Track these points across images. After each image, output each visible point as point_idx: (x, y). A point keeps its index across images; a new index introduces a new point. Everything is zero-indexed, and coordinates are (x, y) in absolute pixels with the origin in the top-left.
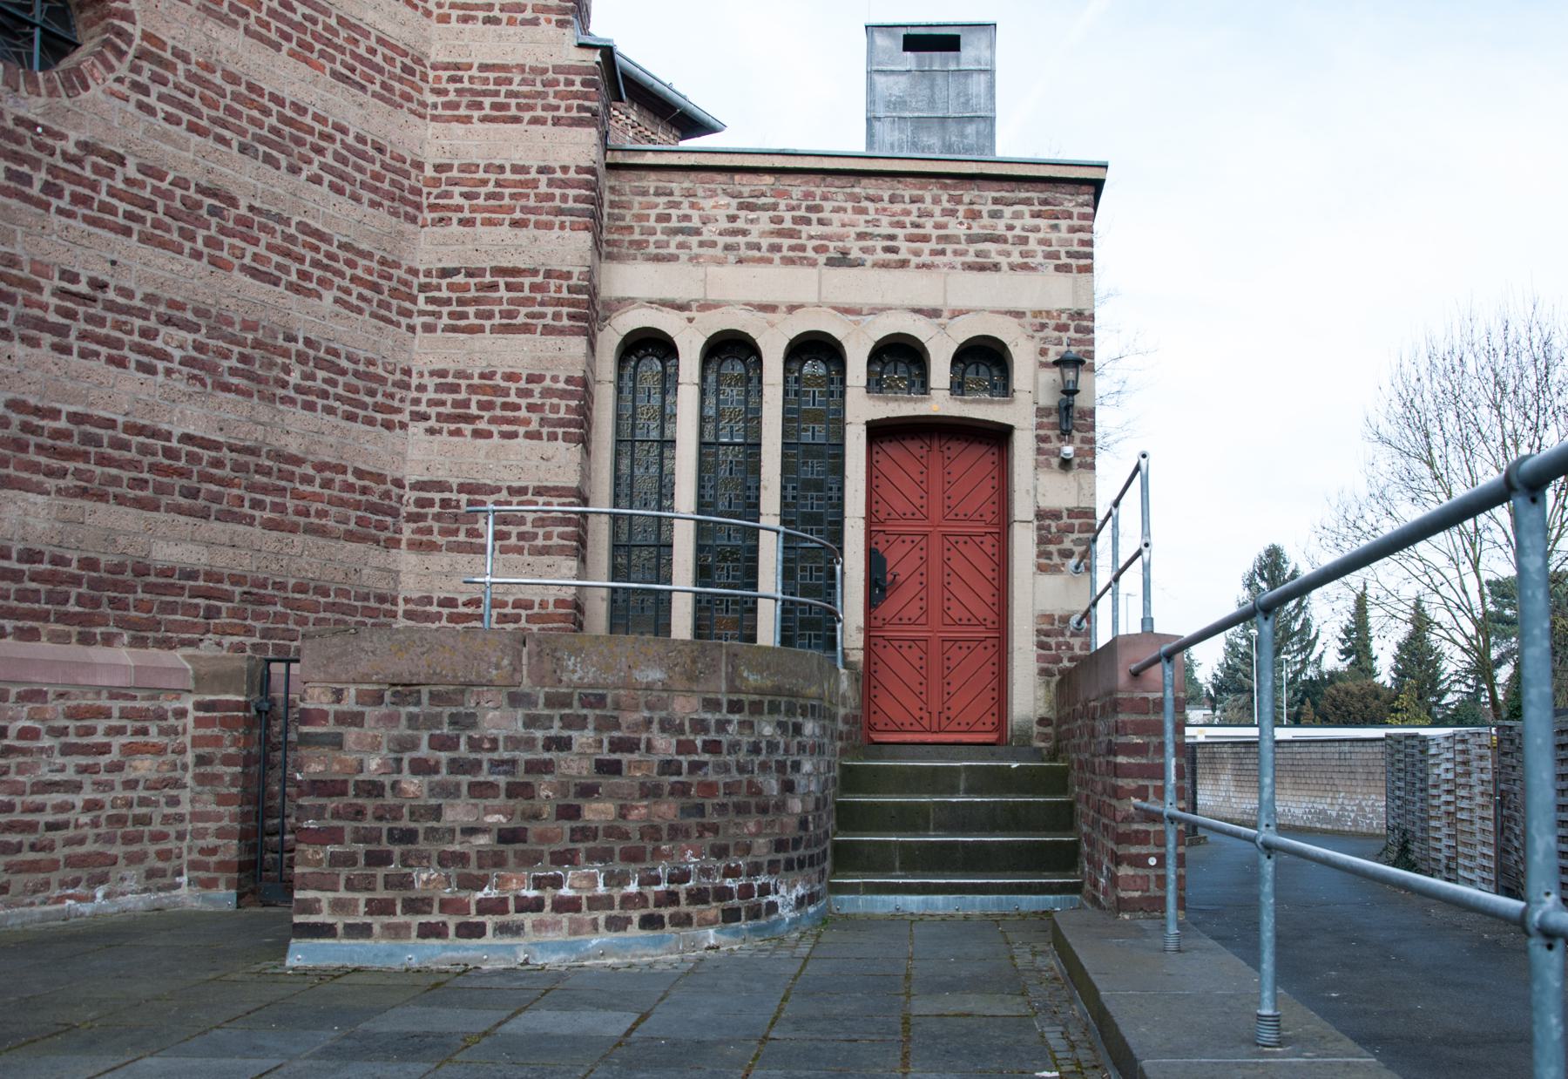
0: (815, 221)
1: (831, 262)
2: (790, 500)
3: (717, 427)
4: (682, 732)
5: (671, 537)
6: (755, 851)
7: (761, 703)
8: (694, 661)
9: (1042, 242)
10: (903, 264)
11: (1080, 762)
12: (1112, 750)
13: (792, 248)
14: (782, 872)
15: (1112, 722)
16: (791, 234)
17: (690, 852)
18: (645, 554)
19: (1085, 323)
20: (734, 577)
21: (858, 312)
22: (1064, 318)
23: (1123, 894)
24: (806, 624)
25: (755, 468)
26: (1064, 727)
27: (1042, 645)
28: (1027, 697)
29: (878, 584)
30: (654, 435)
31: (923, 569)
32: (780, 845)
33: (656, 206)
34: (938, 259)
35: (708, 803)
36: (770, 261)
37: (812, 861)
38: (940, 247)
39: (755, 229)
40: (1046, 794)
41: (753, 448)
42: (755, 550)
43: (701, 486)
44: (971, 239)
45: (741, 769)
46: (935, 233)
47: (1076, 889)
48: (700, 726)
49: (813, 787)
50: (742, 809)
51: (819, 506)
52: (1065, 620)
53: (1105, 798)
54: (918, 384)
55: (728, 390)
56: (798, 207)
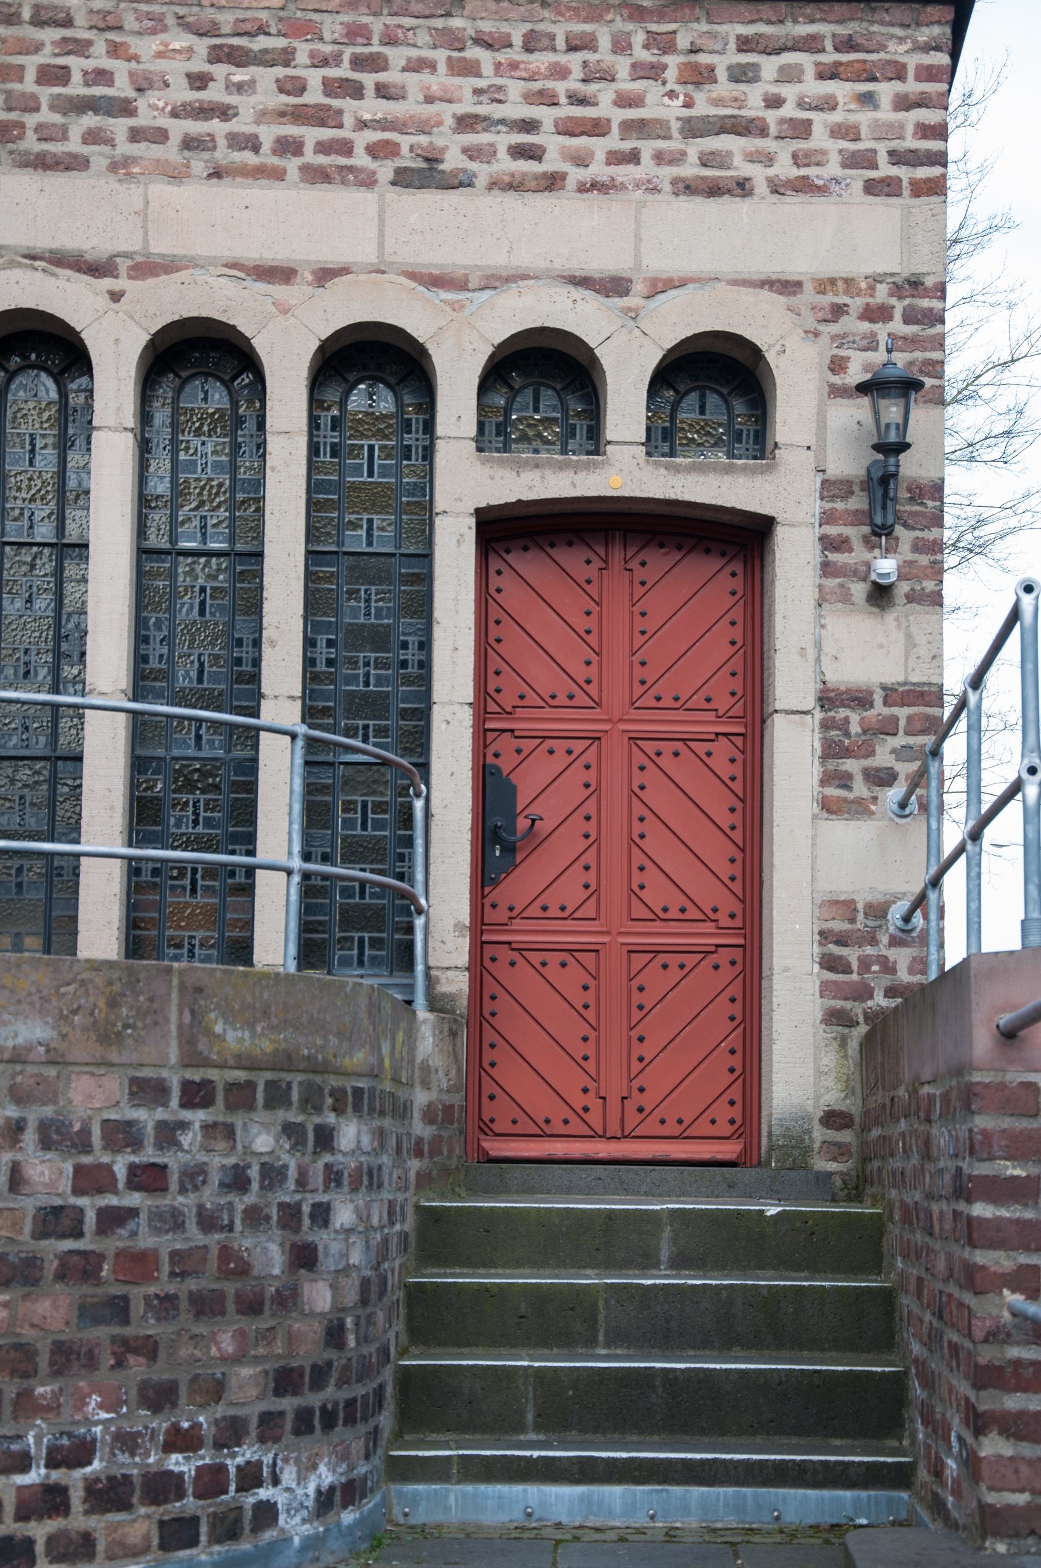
0: (370, 91)
1: (403, 179)
2: (321, 667)
3: (173, 519)
4: (86, 1147)
5: (80, 741)
6: (233, 1393)
7: (251, 1085)
8: (113, 1003)
9: (838, 132)
10: (552, 182)
11: (904, 1205)
12: (964, 1189)
13: (323, 148)
14: (288, 1438)
15: (962, 1130)
16: (321, 117)
17: (95, 1399)
18: (24, 774)
19: (925, 303)
20: (209, 823)
21: (459, 284)
22: (882, 293)
23: (991, 1498)
24: (351, 918)
25: (250, 602)
26: (876, 1132)
27: (830, 963)
28: (802, 1070)
29: (499, 839)
30: (45, 532)
31: (590, 808)
32: (285, 1381)
33: (37, 48)
34: (624, 172)
35: (137, 1294)
36: (278, 175)
37: (352, 1413)
38: (627, 145)
39: (246, 105)
40: (837, 1269)
41: (248, 562)
42: (250, 767)
43: (141, 638)
44: (693, 129)
45: (208, 1222)
46: (618, 115)
47: (898, 1477)
48: (121, 1135)
49: (356, 1257)
50: (206, 1306)
51: (380, 681)
52: (878, 911)
53: (952, 1289)
54: (581, 433)
55: (196, 442)
56: (334, 60)
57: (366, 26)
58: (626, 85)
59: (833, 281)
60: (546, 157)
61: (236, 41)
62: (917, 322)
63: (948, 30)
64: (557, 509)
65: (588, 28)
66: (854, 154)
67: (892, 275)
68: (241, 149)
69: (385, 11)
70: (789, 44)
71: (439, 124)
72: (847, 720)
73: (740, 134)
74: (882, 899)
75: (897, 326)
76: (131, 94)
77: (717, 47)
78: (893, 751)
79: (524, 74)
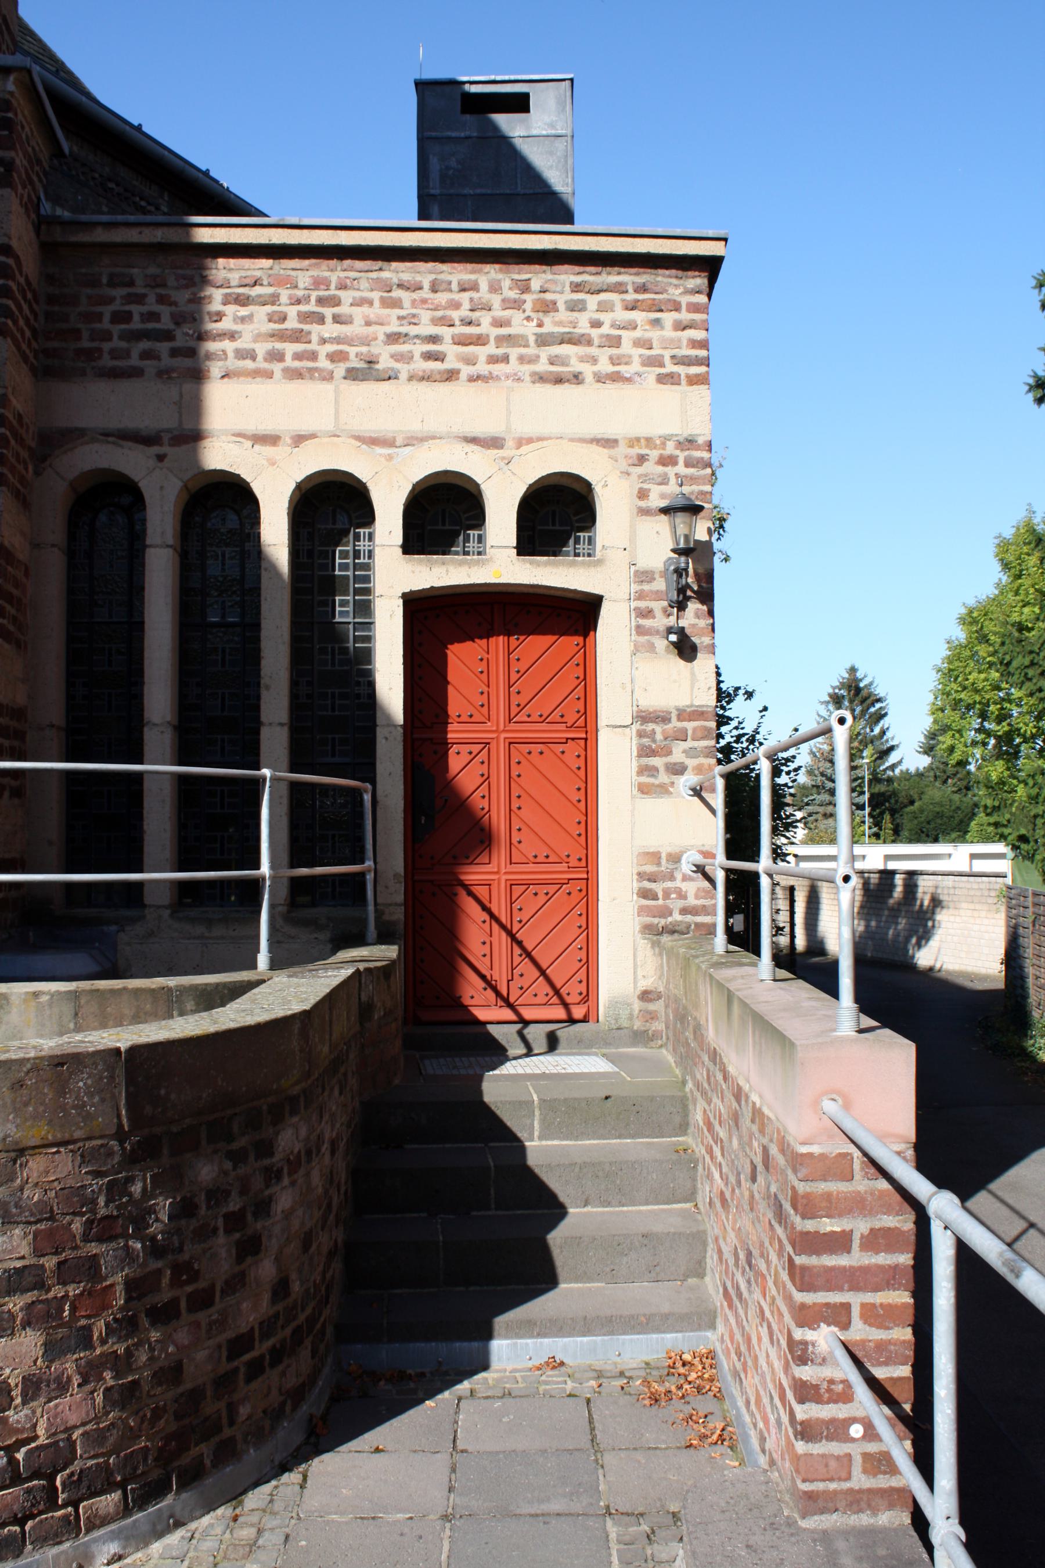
0: (329, 319)
1: (352, 375)
10: (451, 376)
13: (298, 356)
16: (298, 336)
22: (670, 449)
27: (645, 894)
33: (111, 300)
34: (498, 369)
36: (269, 375)
38: (500, 351)
44: (543, 341)
57: (326, 278)
58: (499, 313)
59: (638, 440)
60: (447, 359)
61: (241, 290)
62: (693, 466)
63: (706, 281)
64: (458, 591)
65: (473, 277)
66: (649, 357)
67: (676, 435)
68: (244, 359)
69: (339, 268)
70: (605, 288)
71: (376, 339)
72: (653, 732)
73: (575, 344)
74: (677, 850)
75: (681, 468)
76: (172, 326)
77: (558, 289)
78: (684, 752)
79: (431, 307)
